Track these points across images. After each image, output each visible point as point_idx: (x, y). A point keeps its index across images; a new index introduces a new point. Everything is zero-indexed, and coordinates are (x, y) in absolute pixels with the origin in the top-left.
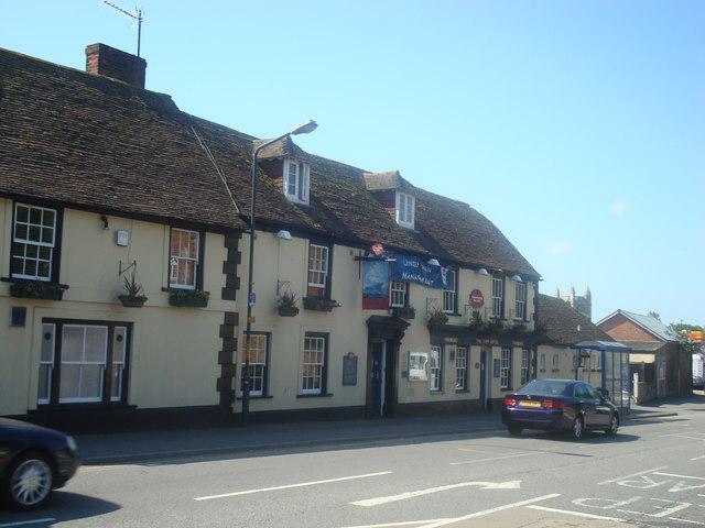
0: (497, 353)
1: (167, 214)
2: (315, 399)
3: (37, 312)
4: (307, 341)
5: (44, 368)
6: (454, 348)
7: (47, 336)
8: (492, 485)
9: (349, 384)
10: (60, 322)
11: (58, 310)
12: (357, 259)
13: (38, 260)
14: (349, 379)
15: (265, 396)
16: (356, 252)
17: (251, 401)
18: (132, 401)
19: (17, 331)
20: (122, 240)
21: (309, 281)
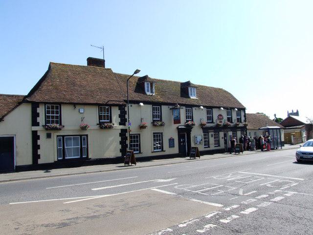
0: (230, 133)
1: (95, 102)
2: (137, 155)
3: (54, 135)
4: (154, 136)
5: (58, 150)
6: (213, 133)
7: (60, 140)
8: (95, 189)
9: (171, 147)
10: (63, 136)
11: (61, 133)
12: (171, 109)
13: (51, 119)
14: (171, 144)
15: (140, 153)
16: (171, 107)
17: (90, 157)
18: (90, 157)
19: (49, 140)
20: (82, 111)
21: (187, 118)
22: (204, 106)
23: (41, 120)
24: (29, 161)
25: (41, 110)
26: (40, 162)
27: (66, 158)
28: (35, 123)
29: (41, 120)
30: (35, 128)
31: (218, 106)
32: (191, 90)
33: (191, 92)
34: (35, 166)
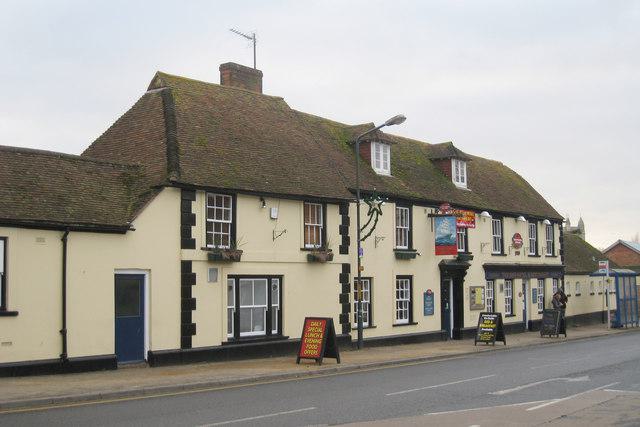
1: (301, 193)
6: (503, 281)
7: (230, 288)
8: (502, 392)
10: (237, 277)
11: (238, 269)
12: (430, 216)
16: (429, 210)
19: (213, 285)
22: (490, 212)
23: (198, 232)
24: (103, 343)
25: (199, 207)
26: (197, 342)
27: (242, 334)
28: (187, 242)
29: (198, 232)
30: (188, 254)
31: (434, 199)
32: (378, 149)
33: (378, 155)
34: (187, 355)
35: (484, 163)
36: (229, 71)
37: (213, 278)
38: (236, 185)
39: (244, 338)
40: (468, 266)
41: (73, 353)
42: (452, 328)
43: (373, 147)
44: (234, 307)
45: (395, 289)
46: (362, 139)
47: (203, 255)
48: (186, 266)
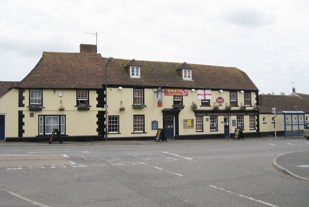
16: (156, 90)
19: (32, 118)
28: (21, 105)
29: (26, 102)
30: (21, 109)
34: (21, 139)
35: (149, 63)
36: (84, 47)
37: (32, 115)
38: (43, 86)
39: (41, 135)
40: (179, 114)
41: (286, 126)
42: (174, 135)
43: (183, 71)
44: (59, 125)
45: (249, 119)
46: (179, 68)
47: (28, 109)
48: (20, 113)
